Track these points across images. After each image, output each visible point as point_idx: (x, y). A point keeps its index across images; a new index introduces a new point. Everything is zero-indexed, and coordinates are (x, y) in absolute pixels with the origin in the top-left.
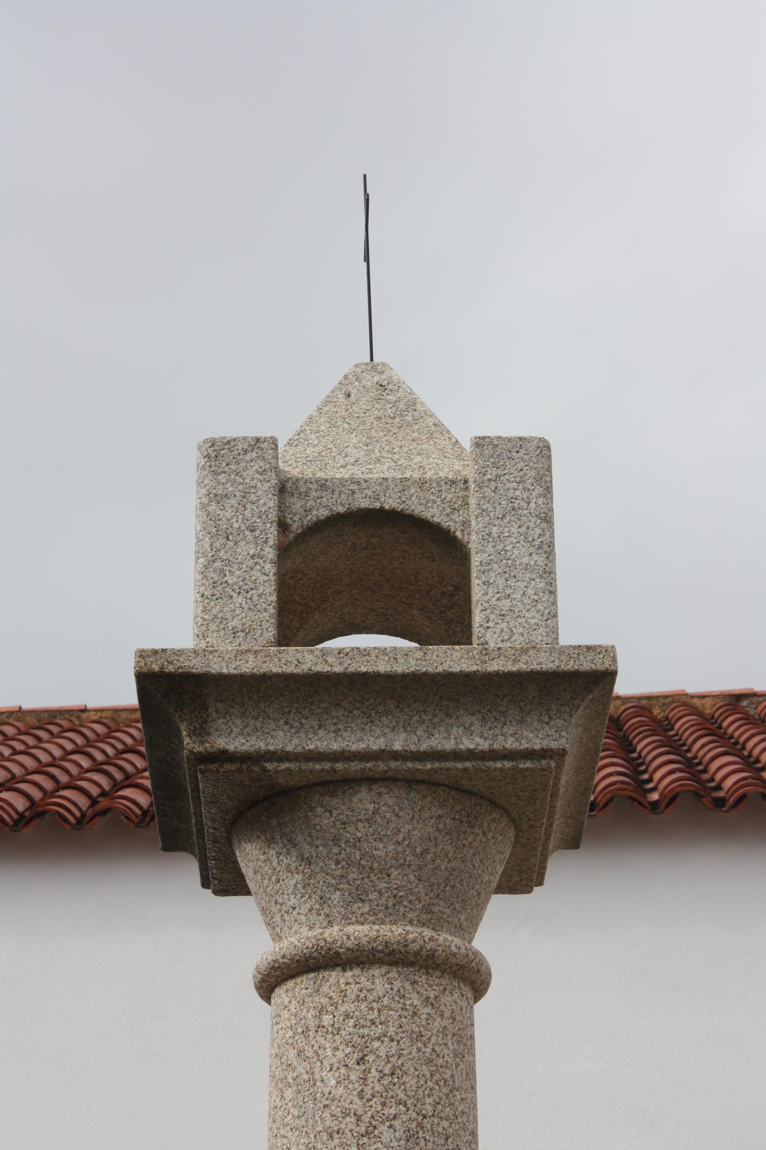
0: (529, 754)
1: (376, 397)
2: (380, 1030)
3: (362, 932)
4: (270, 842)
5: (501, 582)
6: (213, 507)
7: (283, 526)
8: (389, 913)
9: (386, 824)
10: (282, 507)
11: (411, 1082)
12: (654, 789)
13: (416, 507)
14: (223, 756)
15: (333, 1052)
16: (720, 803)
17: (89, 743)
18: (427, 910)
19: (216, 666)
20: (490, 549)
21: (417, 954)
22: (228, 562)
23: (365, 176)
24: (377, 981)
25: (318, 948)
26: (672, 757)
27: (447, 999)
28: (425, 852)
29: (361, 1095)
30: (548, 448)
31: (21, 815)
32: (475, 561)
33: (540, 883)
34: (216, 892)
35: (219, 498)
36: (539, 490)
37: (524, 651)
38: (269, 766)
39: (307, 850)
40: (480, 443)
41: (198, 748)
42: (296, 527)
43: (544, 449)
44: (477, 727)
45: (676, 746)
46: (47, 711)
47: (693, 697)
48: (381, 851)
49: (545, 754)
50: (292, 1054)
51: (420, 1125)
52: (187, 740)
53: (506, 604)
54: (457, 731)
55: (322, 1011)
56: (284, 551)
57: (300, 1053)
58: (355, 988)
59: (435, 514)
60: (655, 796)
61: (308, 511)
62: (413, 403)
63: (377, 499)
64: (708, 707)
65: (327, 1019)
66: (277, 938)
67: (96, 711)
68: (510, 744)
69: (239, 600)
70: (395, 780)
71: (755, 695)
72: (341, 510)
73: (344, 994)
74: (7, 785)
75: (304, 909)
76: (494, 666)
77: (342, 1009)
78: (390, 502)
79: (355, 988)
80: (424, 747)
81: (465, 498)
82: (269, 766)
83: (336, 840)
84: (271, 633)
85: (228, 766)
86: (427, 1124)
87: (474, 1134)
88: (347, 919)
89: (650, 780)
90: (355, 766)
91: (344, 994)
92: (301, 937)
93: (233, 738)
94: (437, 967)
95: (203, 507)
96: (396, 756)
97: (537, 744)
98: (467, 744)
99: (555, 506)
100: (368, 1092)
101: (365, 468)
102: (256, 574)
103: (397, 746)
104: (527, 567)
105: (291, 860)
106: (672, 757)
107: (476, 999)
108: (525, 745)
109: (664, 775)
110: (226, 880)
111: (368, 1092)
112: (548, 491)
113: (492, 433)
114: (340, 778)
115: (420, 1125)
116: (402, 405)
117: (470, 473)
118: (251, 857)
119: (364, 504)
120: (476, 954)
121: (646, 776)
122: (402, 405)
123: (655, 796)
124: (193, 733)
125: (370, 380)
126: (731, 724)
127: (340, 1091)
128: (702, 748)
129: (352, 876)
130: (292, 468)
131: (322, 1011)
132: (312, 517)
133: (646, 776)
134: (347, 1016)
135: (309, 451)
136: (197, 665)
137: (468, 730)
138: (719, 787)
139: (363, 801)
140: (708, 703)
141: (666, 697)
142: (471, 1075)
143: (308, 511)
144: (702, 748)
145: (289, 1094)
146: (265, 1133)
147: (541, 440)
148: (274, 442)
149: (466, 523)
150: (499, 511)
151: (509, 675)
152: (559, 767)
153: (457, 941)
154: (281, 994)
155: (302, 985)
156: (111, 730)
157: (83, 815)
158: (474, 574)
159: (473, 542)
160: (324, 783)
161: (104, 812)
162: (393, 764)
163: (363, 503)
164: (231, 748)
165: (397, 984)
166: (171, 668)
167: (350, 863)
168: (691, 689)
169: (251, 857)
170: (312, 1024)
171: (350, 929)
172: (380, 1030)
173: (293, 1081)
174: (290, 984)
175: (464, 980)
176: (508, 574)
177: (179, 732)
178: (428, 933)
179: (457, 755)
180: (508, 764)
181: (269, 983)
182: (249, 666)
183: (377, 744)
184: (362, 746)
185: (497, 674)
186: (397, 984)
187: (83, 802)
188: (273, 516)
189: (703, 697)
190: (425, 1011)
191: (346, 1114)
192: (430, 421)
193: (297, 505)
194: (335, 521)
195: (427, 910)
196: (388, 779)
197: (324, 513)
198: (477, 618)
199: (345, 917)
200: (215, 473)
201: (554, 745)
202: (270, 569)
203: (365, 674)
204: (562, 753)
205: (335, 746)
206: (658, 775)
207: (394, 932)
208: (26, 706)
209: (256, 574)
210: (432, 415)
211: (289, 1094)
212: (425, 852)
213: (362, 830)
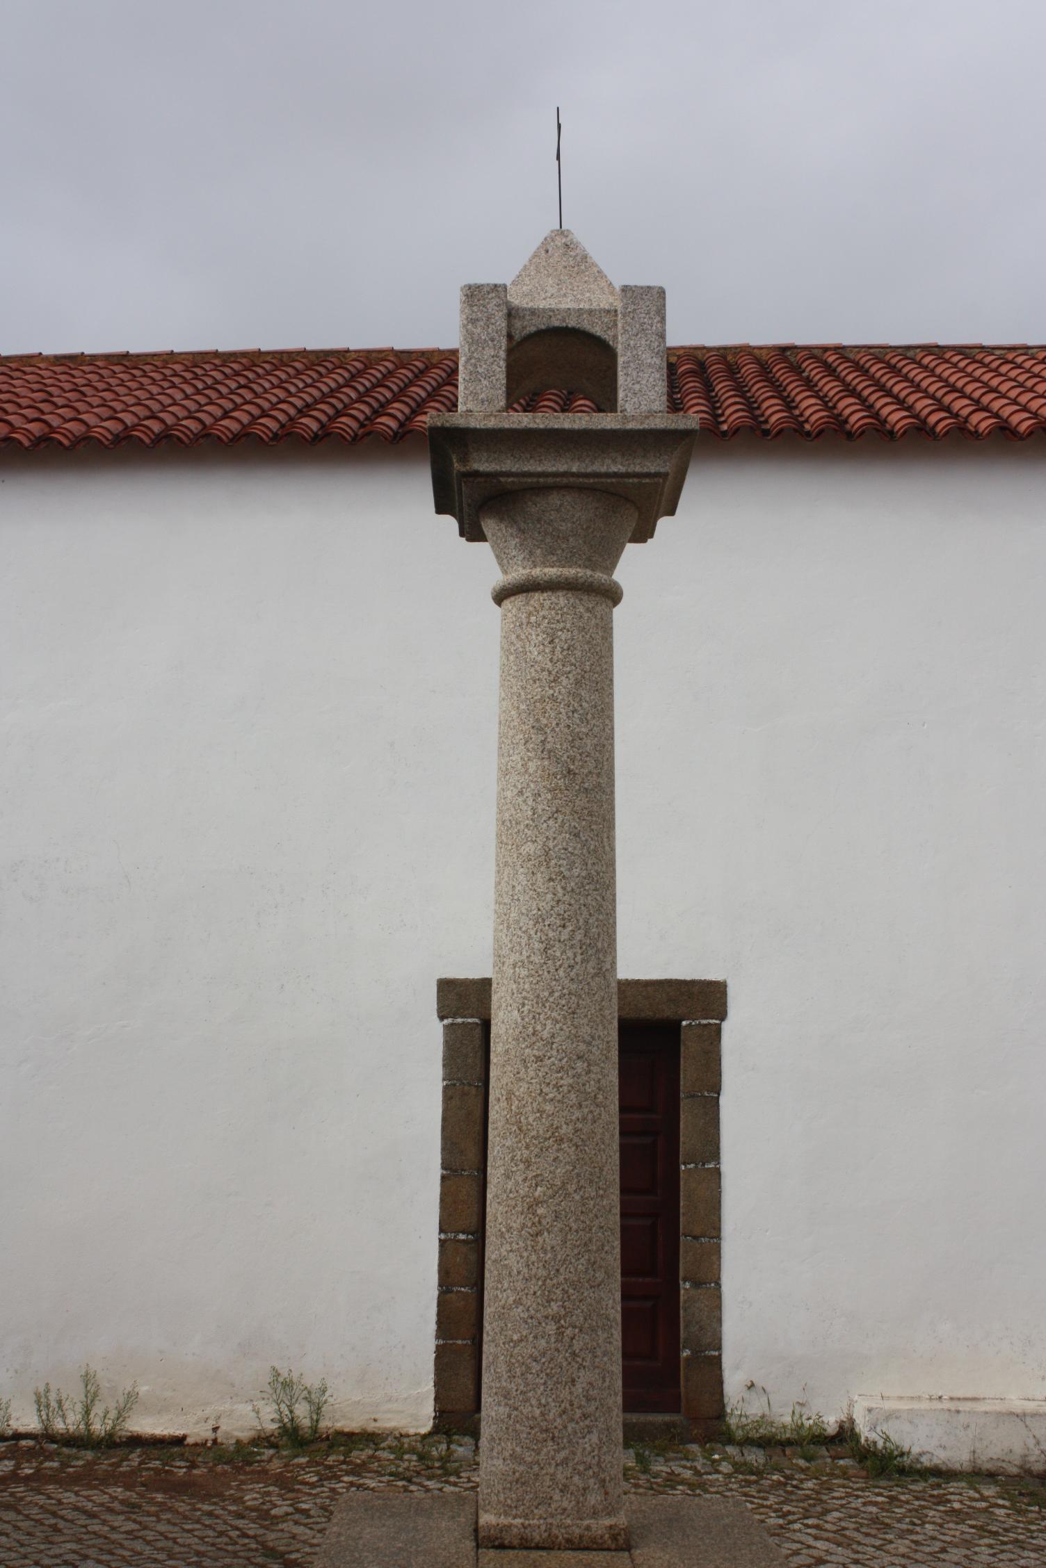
0: (648, 475)
1: (562, 251)
2: (562, 625)
3: (552, 572)
4: (502, 520)
5: (635, 374)
6: (470, 326)
7: (510, 337)
9: (567, 512)
10: (509, 326)
11: (578, 654)
12: (725, 422)
13: (586, 325)
14: (476, 474)
15: (537, 636)
16: (766, 433)
18: (589, 559)
20: (629, 354)
21: (583, 584)
22: (479, 360)
24: (561, 599)
25: (528, 580)
26: (737, 399)
27: (599, 608)
28: (588, 527)
29: (551, 660)
30: (664, 292)
31: (316, 435)
32: (621, 360)
33: (652, 537)
34: (468, 540)
35: (473, 321)
36: (658, 319)
37: (647, 417)
38: (502, 479)
39: (523, 525)
40: (625, 289)
41: (463, 469)
42: (517, 337)
43: (661, 293)
44: (619, 459)
45: (740, 389)
46: (322, 351)
47: (754, 348)
49: (657, 475)
50: (514, 637)
51: (583, 677)
52: (456, 465)
53: (637, 387)
54: (608, 461)
55: (530, 614)
56: (510, 351)
57: (518, 637)
58: (548, 602)
59: (597, 330)
60: (725, 427)
61: (524, 328)
62: (585, 257)
63: (564, 321)
64: (764, 356)
65: (533, 619)
66: (505, 572)
67: (356, 351)
68: (638, 469)
69: (485, 382)
70: (572, 487)
71: (796, 347)
72: (543, 327)
73: (542, 606)
74: (1042, 1548)
75: (521, 557)
76: (630, 426)
77: (541, 614)
78: (572, 323)
79: (548, 602)
80: (589, 470)
81: (615, 321)
82: (502, 479)
83: (539, 521)
84: (503, 403)
85: (479, 479)
86: (587, 676)
87: (611, 680)
88: (544, 564)
89: (722, 415)
90: (550, 480)
91: (542, 606)
92: (519, 573)
93: (483, 464)
94: (593, 591)
95: (464, 326)
96: (573, 475)
97: (653, 470)
98: (614, 469)
99: (668, 328)
100: (555, 658)
101: (557, 300)
102: (495, 367)
103: (574, 470)
104: (650, 365)
105: (513, 531)
106: (737, 399)
107: (615, 605)
108: (646, 470)
109: (733, 413)
110: (472, 532)
111: (555, 658)
112: (663, 320)
113: (632, 283)
114: (541, 487)
115: (583, 677)
116: (578, 259)
117: (619, 305)
118: (489, 526)
119: (557, 324)
120: (616, 583)
121: (720, 412)
122: (578, 259)
123: (725, 427)
124: (459, 461)
125: (560, 241)
126: (779, 371)
127: (540, 658)
128: (759, 390)
129: (548, 540)
130: (516, 300)
131: (530, 614)
132: (526, 332)
133: (720, 412)
134: (544, 617)
135: (525, 288)
137: (614, 461)
138: (766, 422)
139: (555, 499)
140: (764, 352)
141: (736, 348)
142: (610, 648)
143: (524, 328)
144: (759, 390)
145: (512, 658)
146: (498, 678)
147: (661, 288)
148: (505, 286)
149: (615, 337)
150: (635, 331)
151: (639, 431)
152: (664, 482)
153: (605, 577)
154: (507, 603)
155: (519, 600)
156: (366, 367)
157: (356, 435)
158: (619, 369)
159: (620, 349)
160: (532, 489)
161: (369, 434)
162: (571, 479)
163: (556, 323)
164: (481, 469)
165: (572, 601)
166: (448, 425)
167: (546, 534)
168: (752, 343)
169: (489, 526)
170: (525, 621)
171: (546, 570)
172: (562, 625)
173: (513, 650)
174: (512, 599)
175: (608, 597)
176: (639, 369)
177: (451, 460)
178: (589, 573)
179: (607, 475)
180: (636, 480)
181: (501, 596)
182: (492, 423)
183: (562, 467)
184: (554, 469)
185: (631, 431)
186: (572, 601)
187: (354, 425)
188: (504, 332)
189: (760, 348)
190: (587, 615)
191: (543, 670)
192: (595, 270)
193: (518, 324)
194: (540, 334)
195: (589, 559)
197: (533, 329)
198: (621, 394)
199: (543, 563)
200: (471, 306)
201: (662, 470)
202: (503, 364)
203: (557, 430)
204: (666, 475)
205: (539, 469)
206: (728, 412)
207: (570, 572)
208: (309, 348)
209: (495, 367)
210: (597, 266)
211: (512, 658)
212: (588, 527)
213: (553, 515)
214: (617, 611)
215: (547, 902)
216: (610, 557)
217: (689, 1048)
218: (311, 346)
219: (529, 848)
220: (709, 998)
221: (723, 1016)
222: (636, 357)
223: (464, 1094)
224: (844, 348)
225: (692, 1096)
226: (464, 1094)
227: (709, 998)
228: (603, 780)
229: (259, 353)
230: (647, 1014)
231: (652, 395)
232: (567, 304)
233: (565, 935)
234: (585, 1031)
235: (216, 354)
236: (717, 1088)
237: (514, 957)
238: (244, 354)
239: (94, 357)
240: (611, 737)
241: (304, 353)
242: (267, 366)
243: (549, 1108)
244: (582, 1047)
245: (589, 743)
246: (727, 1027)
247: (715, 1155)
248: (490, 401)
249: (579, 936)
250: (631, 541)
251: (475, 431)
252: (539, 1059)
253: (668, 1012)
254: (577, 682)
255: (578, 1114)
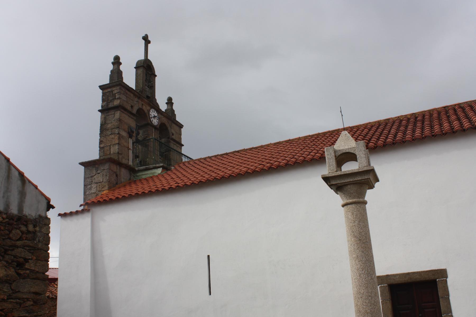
3: (351, 201)
7: (335, 156)
8: (354, 198)
13: (350, 151)
15: (350, 214)
17: (364, 137)
19: (330, 176)
23: (209, 256)
24: (353, 206)
48: (352, 191)
56: (336, 159)
59: (352, 152)
78: (347, 151)
98: (359, 179)
114: (346, 185)
118: (338, 192)
136: (328, 176)
139: (349, 186)
181: (343, 206)
182: (333, 175)
183: (349, 181)
193: (337, 153)
194: (342, 154)
196: (351, 184)
207: (354, 200)
214: (366, 205)
215: (359, 266)
216: (363, 194)
217: (440, 286)
218: (330, 130)
219: (354, 256)
220: (443, 273)
221: (447, 277)
222: (360, 156)
223: (386, 303)
224: (460, 104)
225: (442, 298)
226: (386, 303)
227: (443, 273)
228: (367, 240)
229: (319, 134)
230: (400, 282)
231: (364, 163)
232: (347, 147)
233: (363, 272)
234: (370, 291)
235: (309, 136)
236: (448, 295)
237: (354, 278)
238: (316, 135)
239: (283, 142)
240: (369, 231)
241: (329, 132)
242: (320, 137)
243: (364, 307)
244: (370, 294)
245: (363, 233)
246: (448, 280)
247: (451, 312)
248: (333, 170)
249: (366, 272)
250: (368, 189)
251: (330, 177)
252: (361, 297)
253: (433, 278)
254: (359, 222)
255: (371, 307)
